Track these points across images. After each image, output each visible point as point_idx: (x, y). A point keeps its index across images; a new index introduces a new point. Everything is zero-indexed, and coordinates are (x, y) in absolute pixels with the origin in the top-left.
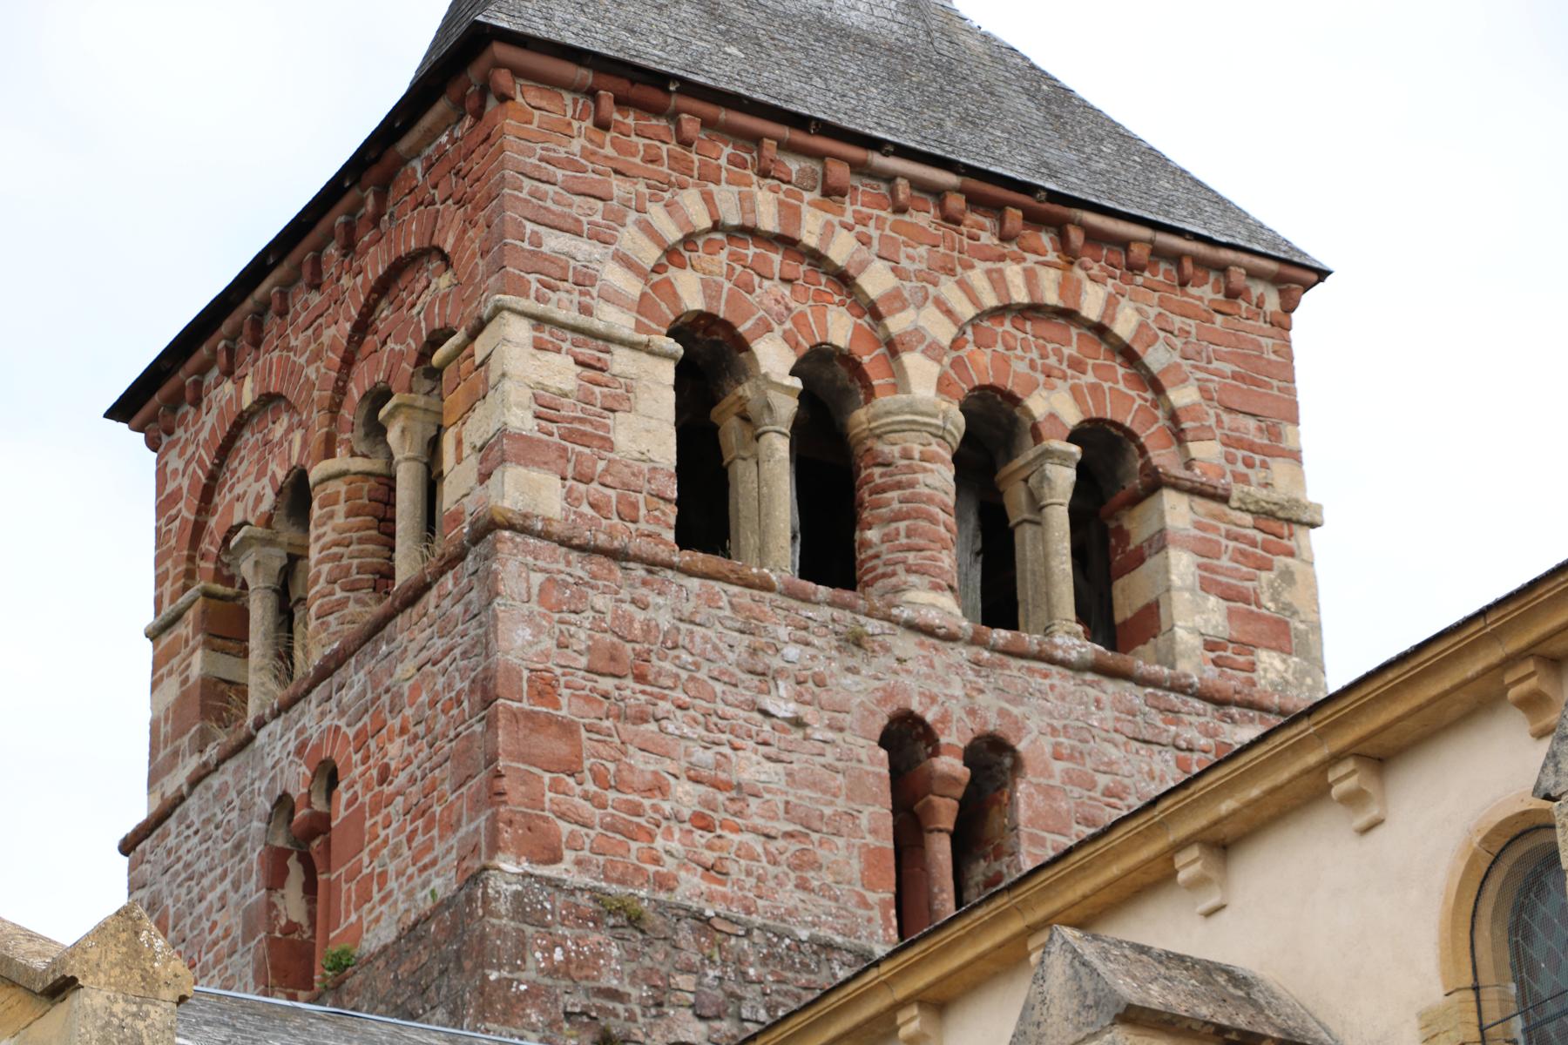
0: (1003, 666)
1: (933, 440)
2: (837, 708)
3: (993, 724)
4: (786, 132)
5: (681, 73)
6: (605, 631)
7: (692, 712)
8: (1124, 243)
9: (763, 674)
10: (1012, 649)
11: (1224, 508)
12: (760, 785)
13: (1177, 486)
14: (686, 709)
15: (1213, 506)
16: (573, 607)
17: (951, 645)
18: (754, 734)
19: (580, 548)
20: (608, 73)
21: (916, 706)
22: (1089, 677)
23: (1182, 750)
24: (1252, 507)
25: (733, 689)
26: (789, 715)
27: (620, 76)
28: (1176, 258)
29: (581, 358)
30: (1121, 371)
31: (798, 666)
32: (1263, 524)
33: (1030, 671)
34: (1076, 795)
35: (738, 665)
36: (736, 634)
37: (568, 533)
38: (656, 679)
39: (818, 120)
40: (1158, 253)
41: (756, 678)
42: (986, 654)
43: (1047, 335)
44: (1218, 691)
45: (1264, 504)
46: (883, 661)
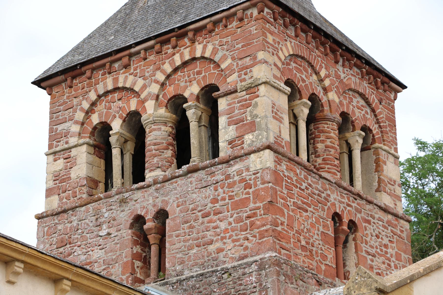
0: (163, 186)
1: (152, 125)
2: (118, 225)
3: (160, 205)
4: (109, 59)
5: (79, 62)
6: (61, 235)
7: (82, 246)
8: (204, 27)
9: (100, 225)
10: (164, 180)
11: (238, 94)
12: (98, 258)
13: (220, 97)
14: (80, 246)
15: (233, 95)
16: (53, 232)
17: (150, 188)
18: (97, 244)
19: (56, 215)
20: (67, 73)
21: (139, 213)
22: (189, 175)
23: (215, 184)
24: (244, 89)
25: (92, 234)
26: (106, 234)
27: (70, 72)
28: (220, 20)
29: (65, 157)
30: (173, 77)
31: (108, 218)
32: (249, 92)
33: (172, 184)
34: (182, 216)
35: (93, 226)
36: (93, 217)
37: (52, 213)
38: (73, 242)
39: (114, 51)
40: (215, 23)
41: (98, 227)
42: (159, 185)
43: (190, 69)
44: (224, 159)
45: (246, 86)
46: (131, 203)
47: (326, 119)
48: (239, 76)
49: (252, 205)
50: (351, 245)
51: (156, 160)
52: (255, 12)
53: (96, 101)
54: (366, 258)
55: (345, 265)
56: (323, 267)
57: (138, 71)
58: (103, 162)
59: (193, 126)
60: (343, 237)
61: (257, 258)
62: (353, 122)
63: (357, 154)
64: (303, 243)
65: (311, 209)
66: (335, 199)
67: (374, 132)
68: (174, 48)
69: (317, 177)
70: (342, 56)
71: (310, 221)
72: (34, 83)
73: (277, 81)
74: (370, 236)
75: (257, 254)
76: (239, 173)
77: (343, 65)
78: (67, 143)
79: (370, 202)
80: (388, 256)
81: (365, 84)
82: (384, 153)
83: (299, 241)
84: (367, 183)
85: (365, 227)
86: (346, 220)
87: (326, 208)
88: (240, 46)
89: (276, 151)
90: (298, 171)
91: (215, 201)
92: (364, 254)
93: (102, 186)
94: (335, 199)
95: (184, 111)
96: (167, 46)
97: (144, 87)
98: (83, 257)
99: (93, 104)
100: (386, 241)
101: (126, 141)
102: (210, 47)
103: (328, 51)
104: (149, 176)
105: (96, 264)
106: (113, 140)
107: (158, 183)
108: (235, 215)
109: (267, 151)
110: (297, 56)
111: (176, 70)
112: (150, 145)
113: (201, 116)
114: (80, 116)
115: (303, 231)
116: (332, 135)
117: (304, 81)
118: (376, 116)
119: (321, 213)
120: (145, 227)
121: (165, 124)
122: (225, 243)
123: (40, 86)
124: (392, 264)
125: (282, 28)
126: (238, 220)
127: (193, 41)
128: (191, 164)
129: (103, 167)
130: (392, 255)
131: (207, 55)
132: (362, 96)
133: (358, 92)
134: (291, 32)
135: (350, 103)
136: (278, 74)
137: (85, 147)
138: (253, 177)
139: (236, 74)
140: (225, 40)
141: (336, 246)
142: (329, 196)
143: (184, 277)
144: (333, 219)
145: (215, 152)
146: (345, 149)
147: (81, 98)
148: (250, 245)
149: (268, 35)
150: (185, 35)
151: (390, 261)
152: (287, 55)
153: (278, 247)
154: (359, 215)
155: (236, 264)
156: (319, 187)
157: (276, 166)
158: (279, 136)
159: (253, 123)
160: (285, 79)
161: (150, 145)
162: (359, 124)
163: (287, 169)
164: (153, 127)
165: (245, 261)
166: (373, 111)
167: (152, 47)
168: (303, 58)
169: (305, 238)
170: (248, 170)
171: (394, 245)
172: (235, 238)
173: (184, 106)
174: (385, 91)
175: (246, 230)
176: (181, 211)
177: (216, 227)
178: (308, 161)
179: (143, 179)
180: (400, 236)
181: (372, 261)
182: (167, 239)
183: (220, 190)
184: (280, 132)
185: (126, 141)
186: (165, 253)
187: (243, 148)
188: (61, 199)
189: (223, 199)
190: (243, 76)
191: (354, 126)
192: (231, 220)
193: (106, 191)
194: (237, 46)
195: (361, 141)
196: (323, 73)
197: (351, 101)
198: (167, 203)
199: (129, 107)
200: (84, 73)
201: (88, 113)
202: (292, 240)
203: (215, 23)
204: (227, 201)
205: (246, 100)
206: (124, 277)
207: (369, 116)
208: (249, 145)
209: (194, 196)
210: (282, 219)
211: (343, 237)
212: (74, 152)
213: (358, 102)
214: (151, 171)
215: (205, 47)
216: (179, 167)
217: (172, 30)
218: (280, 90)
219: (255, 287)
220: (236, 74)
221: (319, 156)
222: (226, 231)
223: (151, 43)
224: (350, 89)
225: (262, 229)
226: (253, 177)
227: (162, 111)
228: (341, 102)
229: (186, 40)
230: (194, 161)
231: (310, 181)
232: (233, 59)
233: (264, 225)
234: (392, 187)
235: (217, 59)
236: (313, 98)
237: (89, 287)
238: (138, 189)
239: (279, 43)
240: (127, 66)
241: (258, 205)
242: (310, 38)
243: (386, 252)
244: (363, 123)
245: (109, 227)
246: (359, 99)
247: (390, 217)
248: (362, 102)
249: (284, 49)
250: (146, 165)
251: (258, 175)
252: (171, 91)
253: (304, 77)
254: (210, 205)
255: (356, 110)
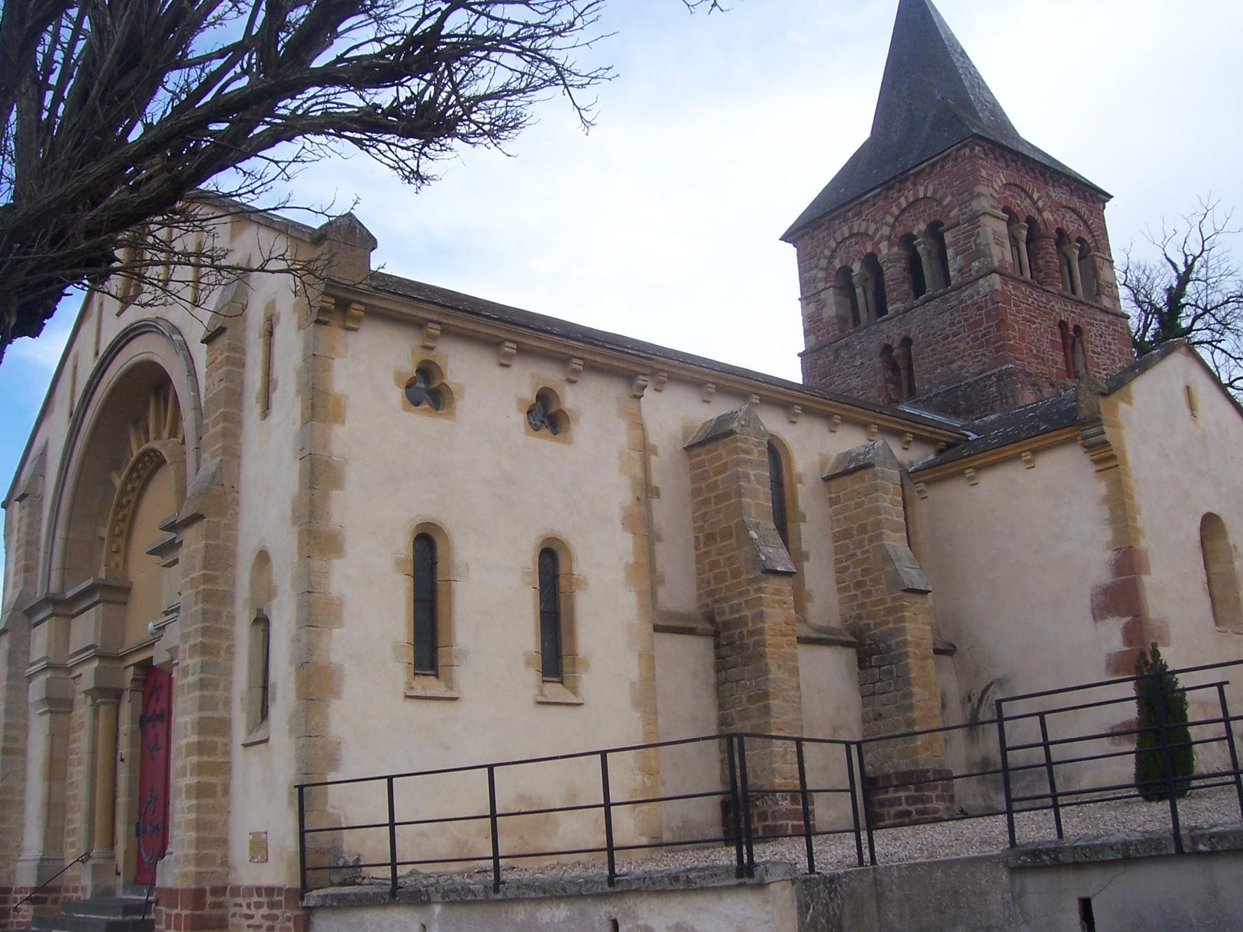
13: (945, 231)
28: (937, 162)
47: (1044, 237)
48: (961, 210)
49: (985, 325)
50: (1079, 347)
51: (895, 293)
52: (967, 151)
53: (836, 247)
54: (1092, 357)
55: (1074, 365)
56: (1055, 371)
57: (869, 217)
58: (848, 301)
59: (924, 259)
60: (1070, 342)
61: (995, 371)
62: (1068, 235)
63: (1076, 264)
64: (1035, 352)
65: (1039, 321)
66: (1059, 309)
67: (1089, 242)
68: (899, 191)
69: (1041, 291)
70: (1051, 177)
71: (1039, 332)
72: (780, 239)
73: (995, 211)
74: (1094, 337)
75: (995, 367)
76: (971, 297)
77: (1053, 186)
78: (815, 288)
79: (1092, 307)
80: (1112, 352)
81: (1075, 199)
82: (1099, 259)
83: (1031, 351)
84: (1087, 289)
85: (1089, 330)
86: (1071, 326)
87: (1052, 318)
88: (957, 183)
89: (1001, 274)
90: (1024, 289)
91: (952, 324)
92: (1090, 354)
93: (850, 322)
94: (1059, 309)
95: (915, 247)
96: (892, 192)
97: (876, 231)
98: (842, 386)
99: (834, 251)
100: (1109, 339)
101: (867, 280)
102: (931, 188)
103: (1038, 175)
104: (891, 309)
105: (855, 391)
106: (855, 280)
107: (900, 314)
108: (972, 335)
109: (994, 275)
110: (1011, 184)
111: (902, 212)
112: (888, 281)
113: (930, 250)
114: (824, 263)
115: (1033, 341)
116: (1051, 250)
117: (1019, 206)
118: (1088, 227)
119: (1048, 324)
120: (894, 354)
121: (899, 260)
122: (965, 361)
123: (786, 241)
124: (1117, 359)
125: (993, 162)
126: (975, 339)
127: (915, 184)
128: (926, 294)
129: (849, 305)
130: (1115, 351)
131: (929, 194)
132: (1074, 211)
133: (1069, 208)
134: (1002, 164)
135: (1063, 219)
136: (995, 204)
137: (831, 290)
138: (984, 299)
139: (957, 209)
140: (943, 180)
141: (1065, 351)
142: (1053, 306)
143: (932, 395)
144: (1060, 326)
145: (947, 281)
146: (1065, 262)
147: (823, 247)
148: (987, 360)
149: (983, 170)
150: (907, 179)
151: (1114, 356)
152: (1001, 185)
153: (1013, 359)
154: (1082, 320)
155: (977, 378)
156: (1044, 300)
157: (1003, 288)
158: (1002, 260)
159: (978, 251)
160: (1001, 207)
161: (888, 281)
162: (1074, 237)
163: (1013, 288)
164: (889, 265)
165: (985, 374)
166: (1085, 222)
167: (879, 194)
168: (1016, 185)
169: (1035, 346)
170: (978, 293)
171: (1116, 341)
172: (973, 355)
173: (915, 243)
174: (1094, 203)
175: (983, 347)
176: (923, 337)
177: (956, 348)
178: (1032, 277)
179: (886, 312)
180: (1121, 333)
181: (1098, 358)
182: (914, 363)
183: (956, 314)
184: (1003, 255)
185: (867, 280)
186: (913, 374)
187: (971, 275)
188: (817, 337)
189: (959, 322)
190: (964, 210)
191: (1069, 240)
192: (968, 340)
193: (855, 326)
194: (955, 184)
195: (1077, 252)
196: (1035, 196)
197: (1064, 216)
198: (910, 331)
199: (866, 250)
200: (823, 224)
201: (831, 259)
202: (1025, 351)
203: (933, 165)
204: (963, 323)
205: (969, 231)
206: (881, 399)
207: (1082, 228)
208: (977, 272)
209: (934, 322)
210: (1014, 334)
211: (1070, 342)
212: (823, 295)
213: (1071, 217)
214: (892, 304)
215: (926, 189)
216: (917, 298)
217: (895, 177)
218: (998, 218)
219: (996, 397)
220: (957, 209)
221: (1041, 272)
222: (965, 350)
223: (878, 190)
224: (1063, 207)
225: (997, 345)
226: (984, 299)
227: (895, 249)
228: (1055, 220)
229: (909, 184)
230: (929, 291)
231: (1035, 296)
232: (953, 195)
233: (998, 342)
234: (1110, 290)
235: (938, 196)
236: (1030, 220)
237: (497, 336)
238: (883, 321)
239: (992, 176)
240: (859, 214)
241: (990, 324)
242: (1020, 167)
243: (1110, 349)
244: (1077, 235)
245: (862, 358)
246: (1072, 214)
247: (1111, 317)
248: (1074, 216)
249: (998, 180)
250: (887, 299)
251: (988, 297)
252: (900, 230)
253: (1019, 202)
254: (948, 329)
255: (1071, 225)
